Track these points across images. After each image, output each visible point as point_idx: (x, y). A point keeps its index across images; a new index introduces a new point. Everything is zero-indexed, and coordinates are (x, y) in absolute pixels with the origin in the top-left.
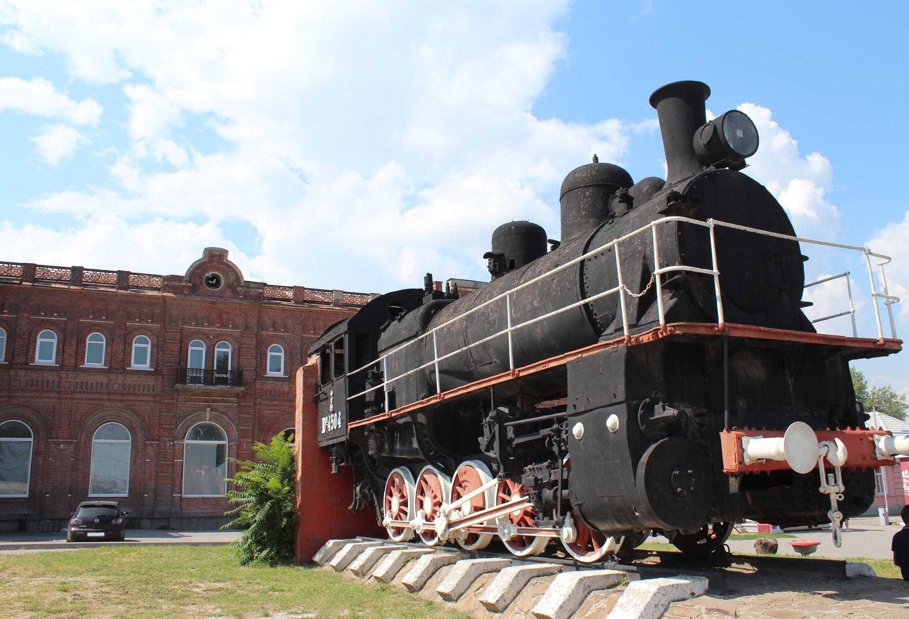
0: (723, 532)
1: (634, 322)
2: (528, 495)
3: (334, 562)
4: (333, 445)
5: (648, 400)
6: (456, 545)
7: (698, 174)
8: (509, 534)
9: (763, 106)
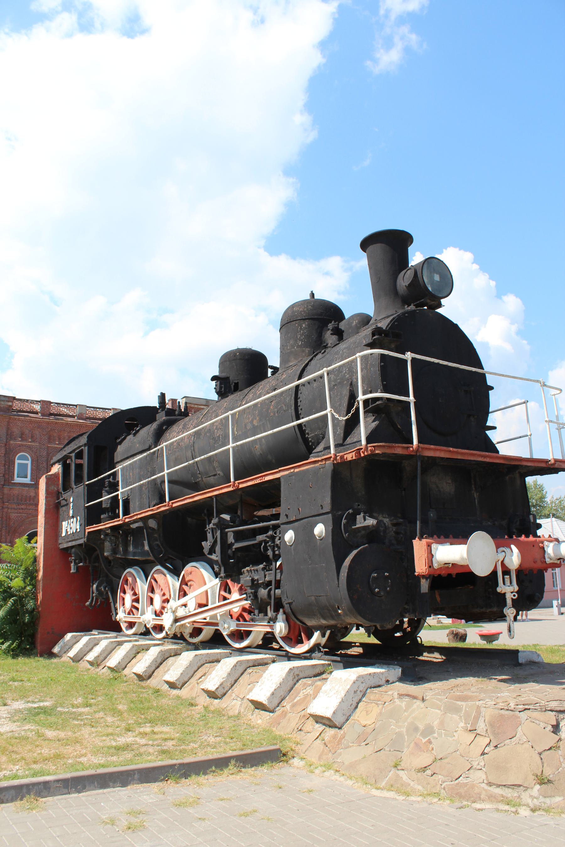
0: (417, 625)
1: (341, 442)
2: (246, 594)
3: (72, 653)
4: (72, 547)
5: (351, 511)
6: (182, 638)
7: (400, 312)
8: (228, 628)
9: (466, 250)
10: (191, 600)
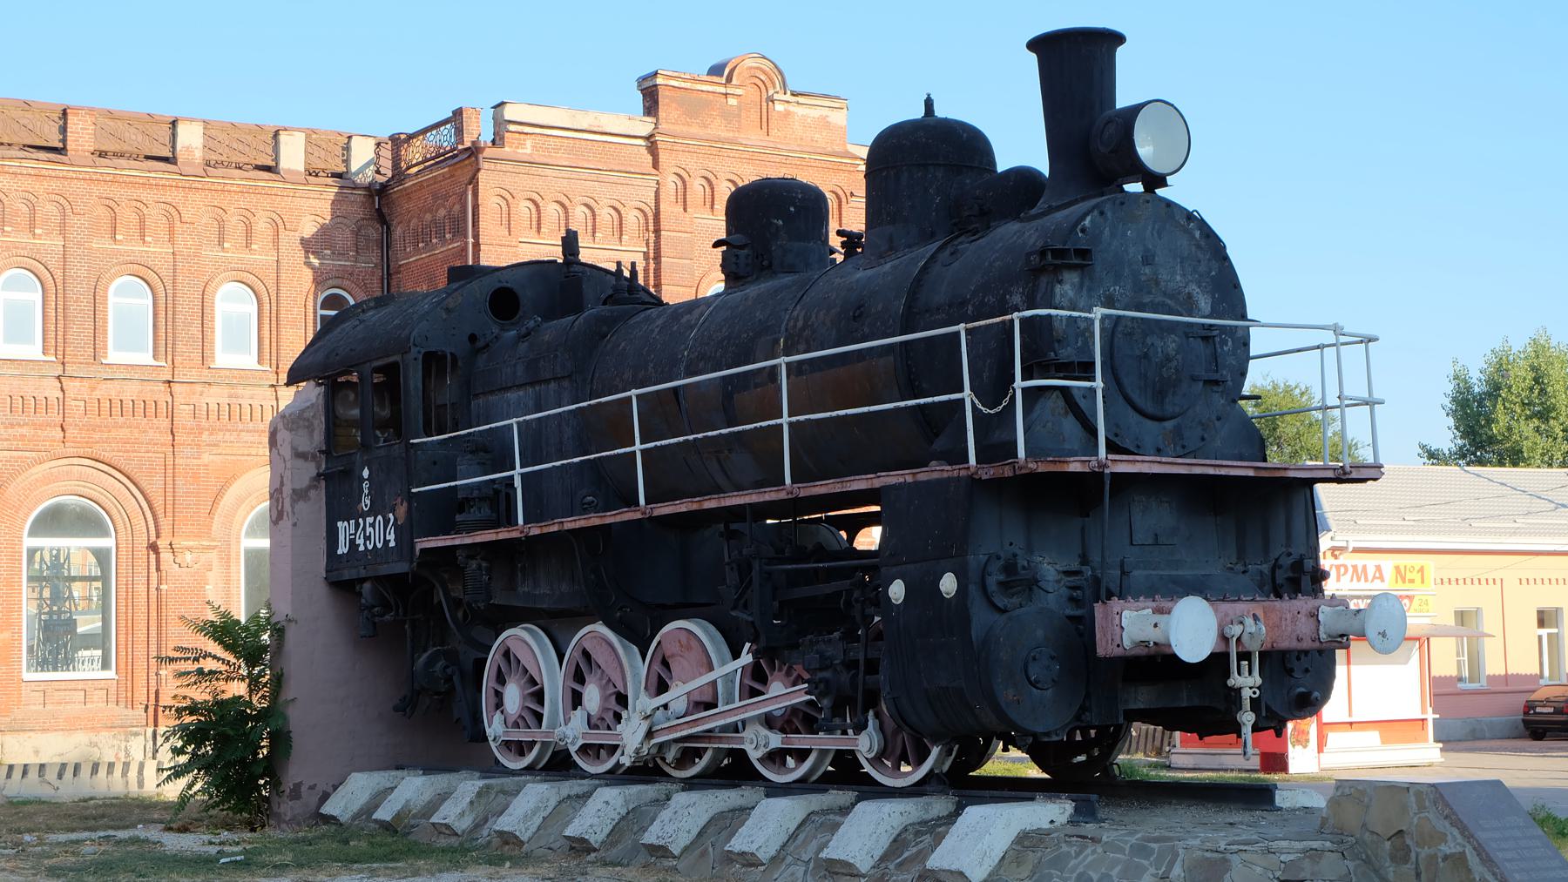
10: (677, 695)
